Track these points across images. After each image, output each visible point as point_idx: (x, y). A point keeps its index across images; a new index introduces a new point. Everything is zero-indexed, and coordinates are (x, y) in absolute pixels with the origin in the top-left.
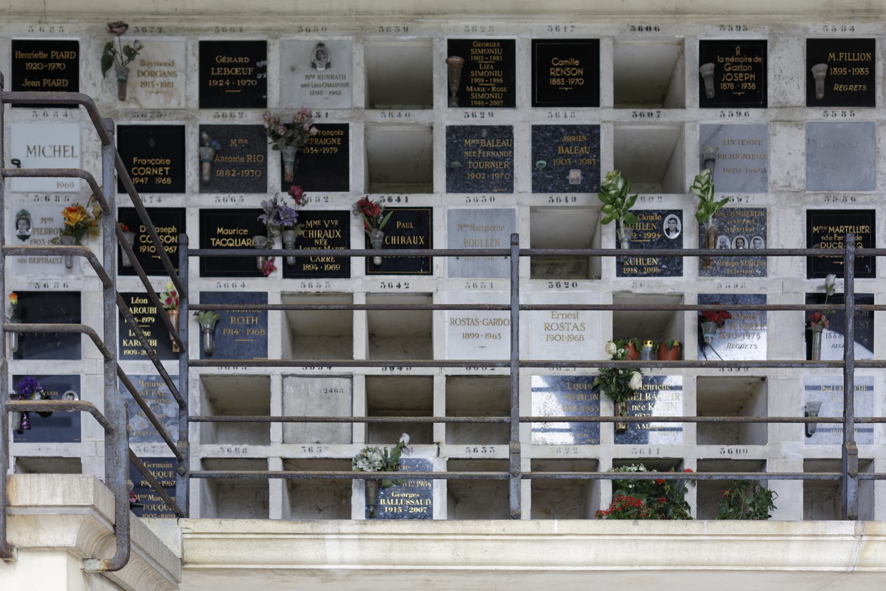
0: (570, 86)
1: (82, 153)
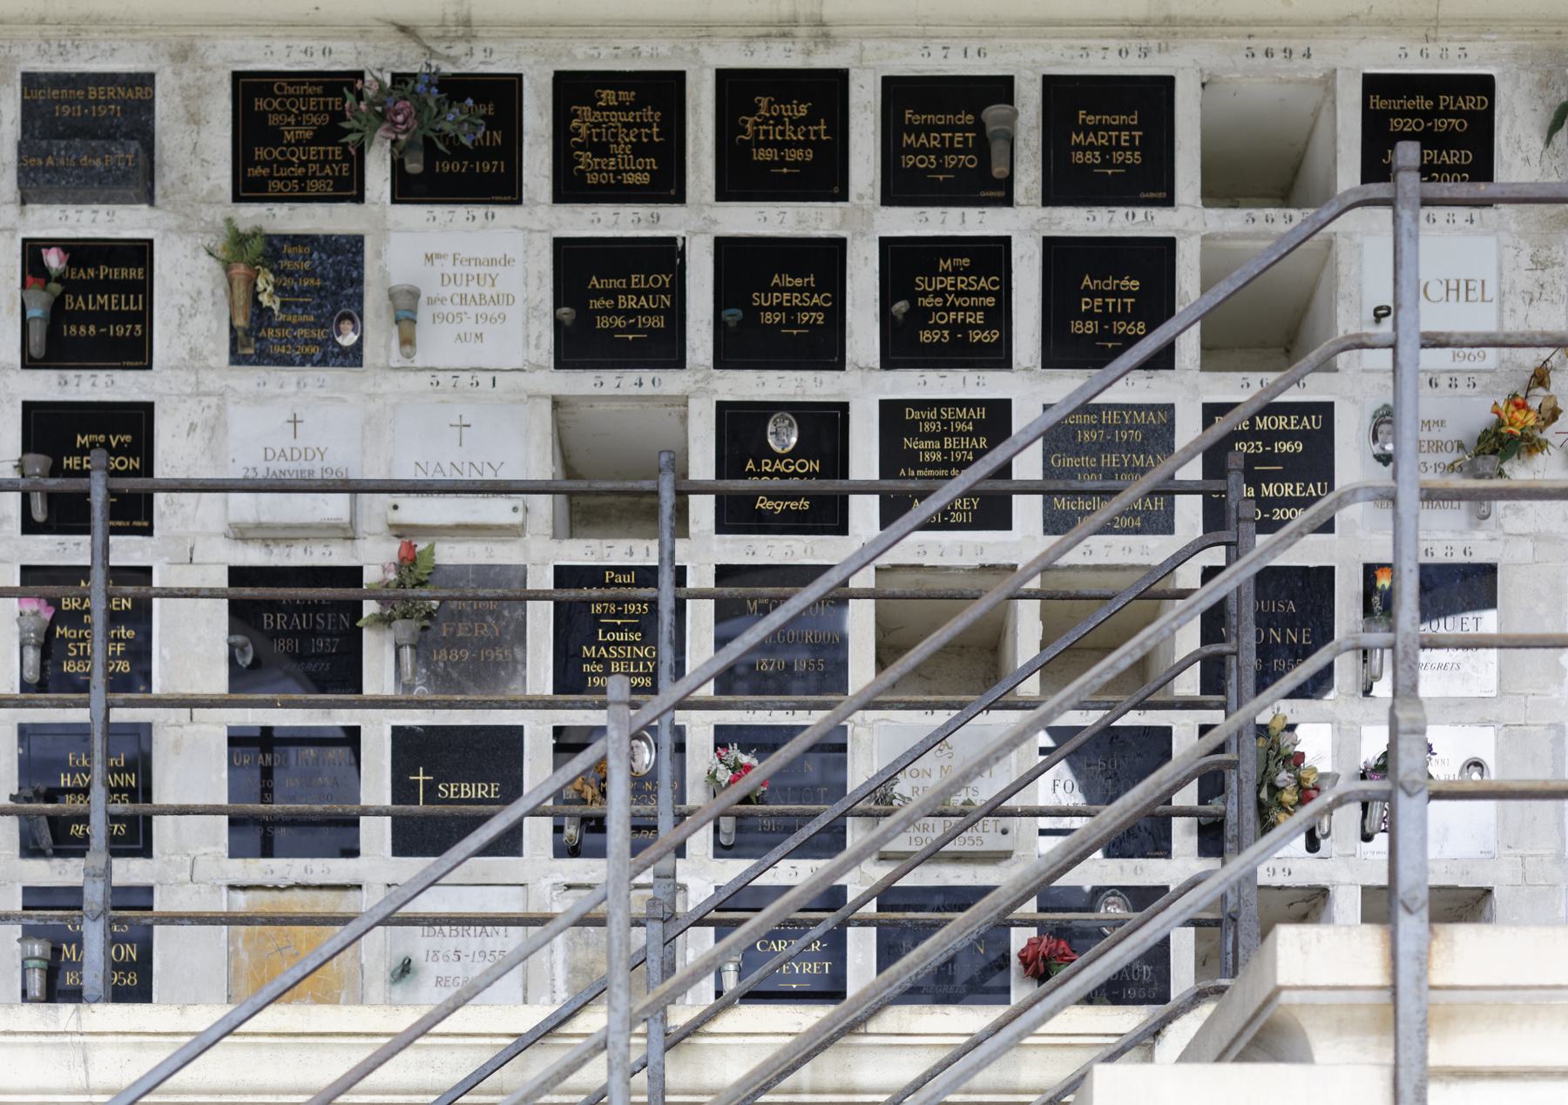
0: (948, 171)
1: (1502, 294)
